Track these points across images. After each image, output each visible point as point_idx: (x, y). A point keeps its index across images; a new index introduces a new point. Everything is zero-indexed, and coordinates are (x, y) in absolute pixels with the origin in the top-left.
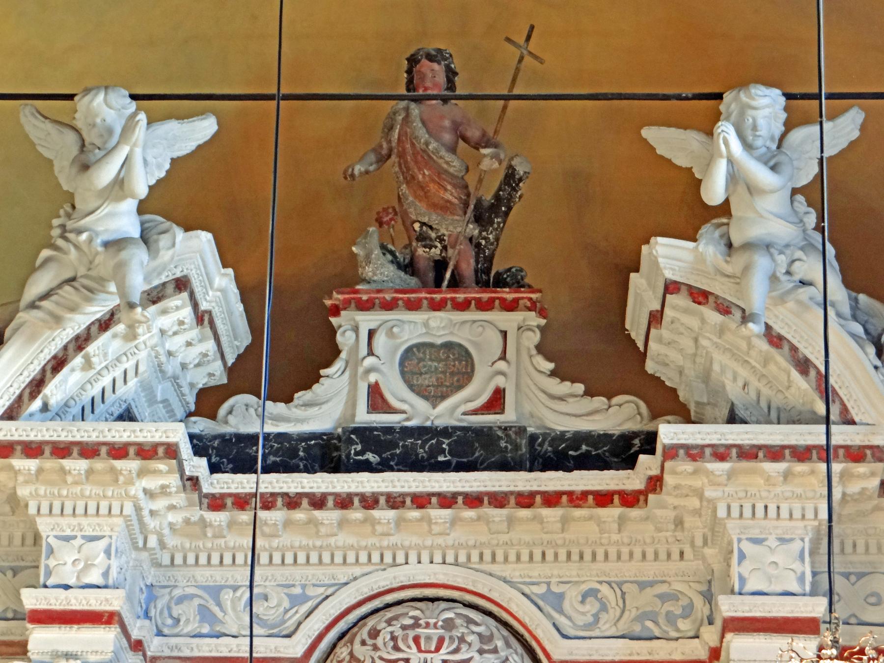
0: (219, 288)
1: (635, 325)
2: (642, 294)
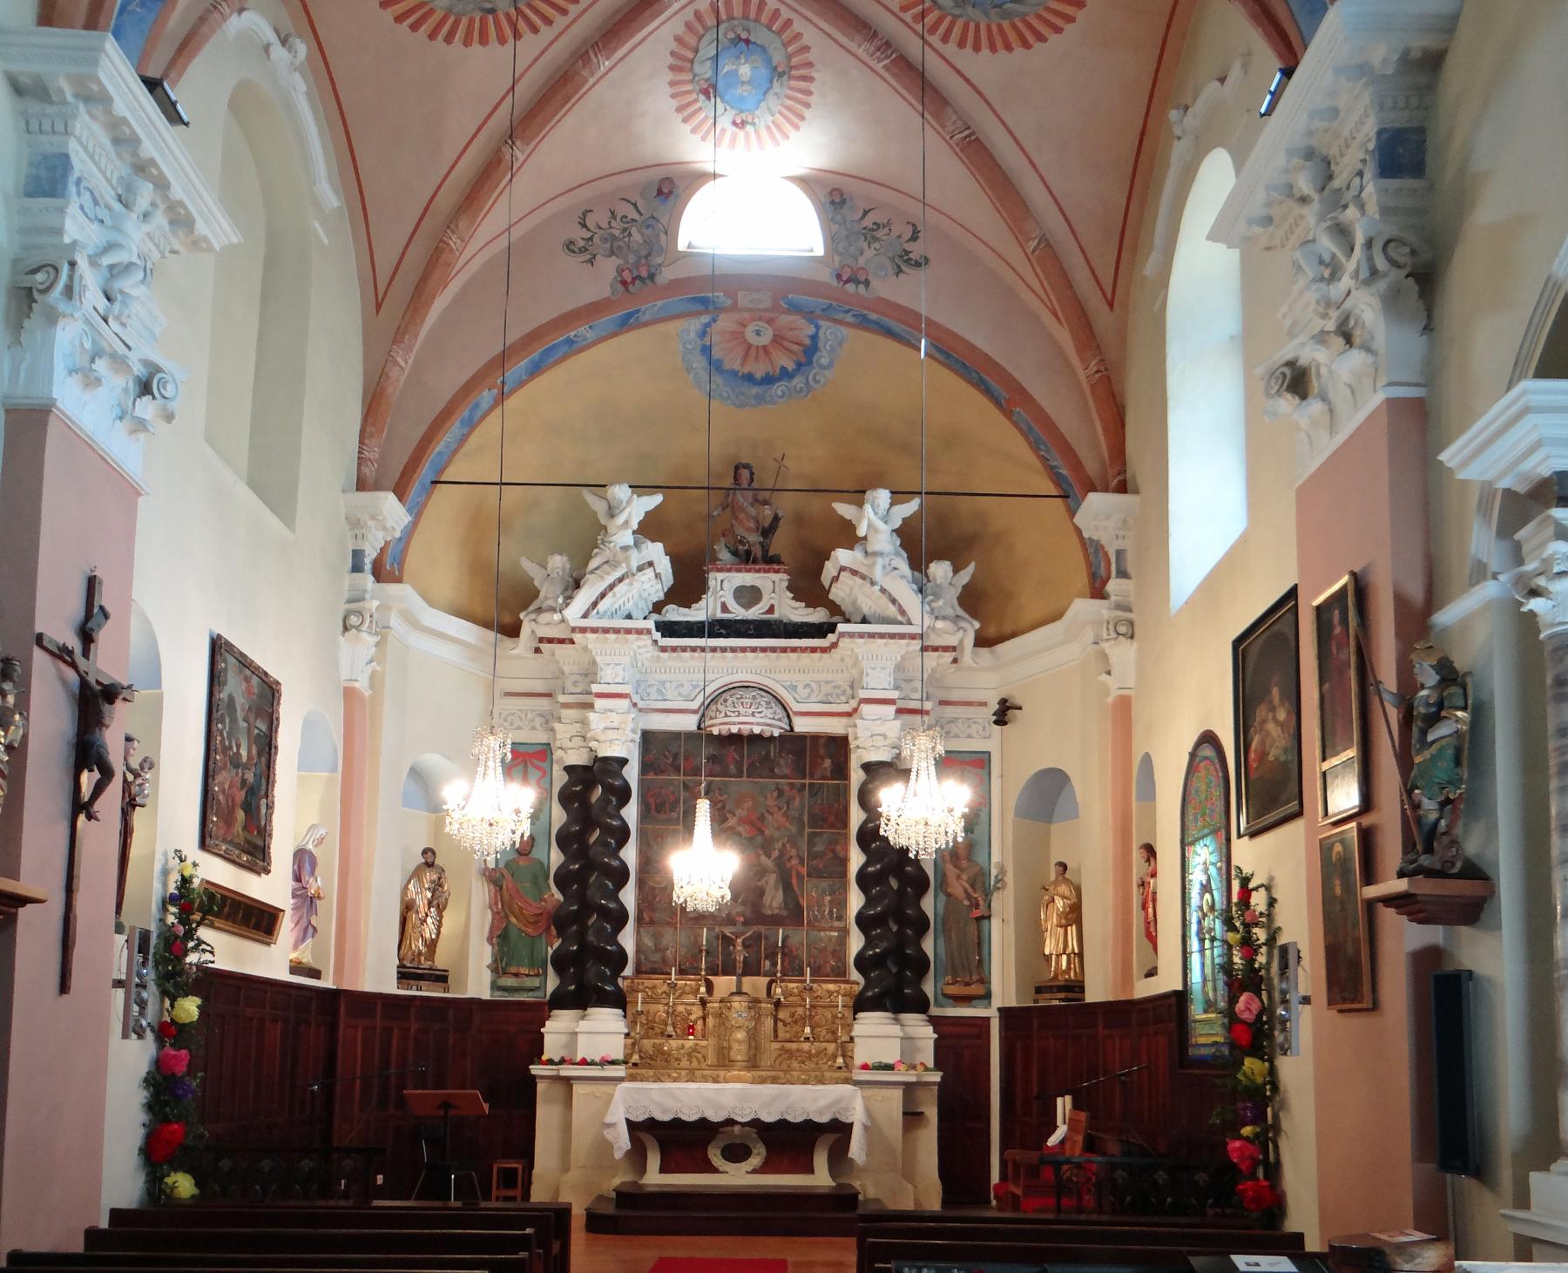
0: (664, 565)
1: (826, 578)
2: (829, 569)
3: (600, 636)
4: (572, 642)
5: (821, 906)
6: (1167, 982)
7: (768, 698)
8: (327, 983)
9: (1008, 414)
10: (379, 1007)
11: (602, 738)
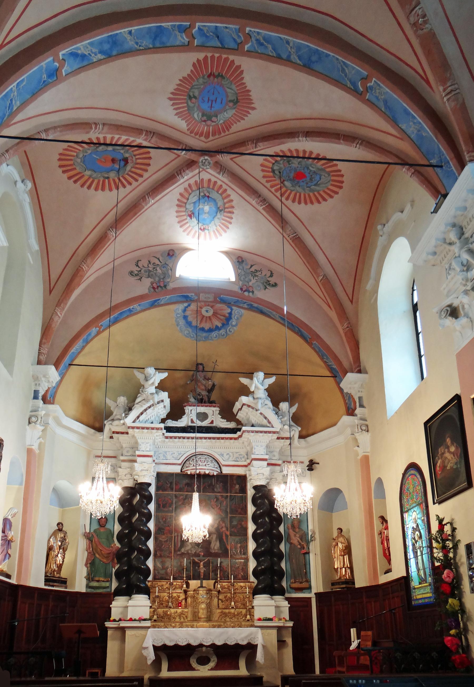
0: (167, 402)
1: (235, 410)
2: (237, 405)
3: (141, 430)
4: (127, 433)
5: (236, 548)
6: (398, 572)
7: (211, 459)
8: (13, 581)
9: (310, 344)
10: (36, 595)
11: (140, 474)
